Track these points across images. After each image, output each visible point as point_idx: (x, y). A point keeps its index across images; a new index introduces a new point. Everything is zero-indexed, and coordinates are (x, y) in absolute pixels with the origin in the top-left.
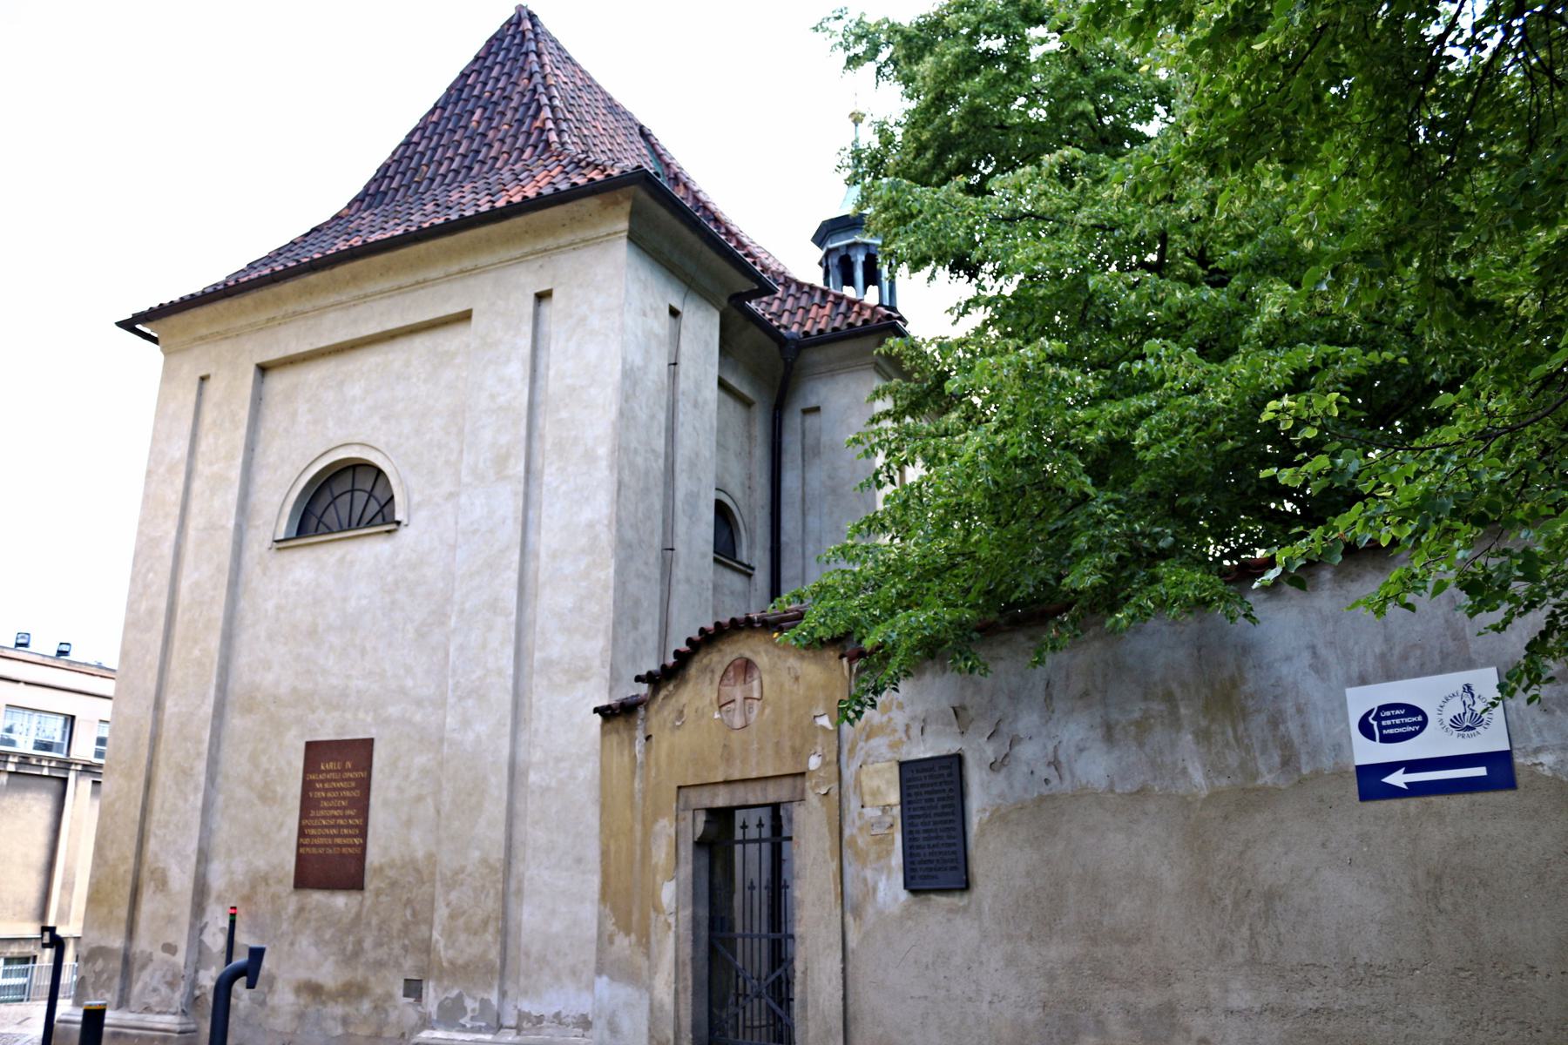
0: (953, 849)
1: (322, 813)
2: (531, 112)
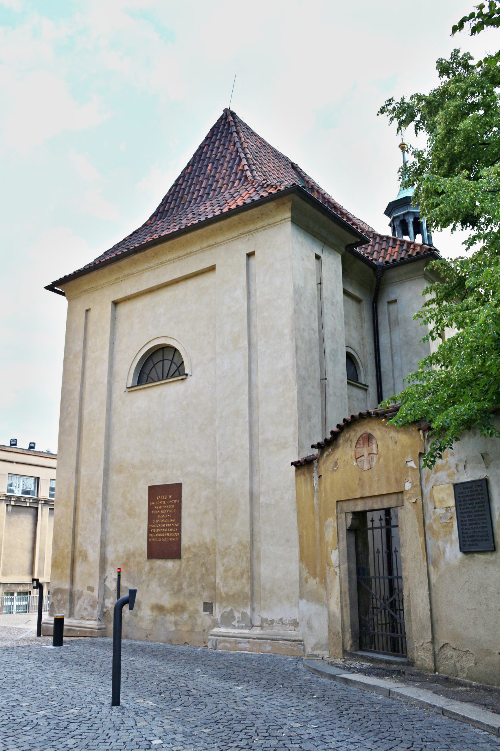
0: (486, 529)
1: (159, 521)
2: (236, 162)
